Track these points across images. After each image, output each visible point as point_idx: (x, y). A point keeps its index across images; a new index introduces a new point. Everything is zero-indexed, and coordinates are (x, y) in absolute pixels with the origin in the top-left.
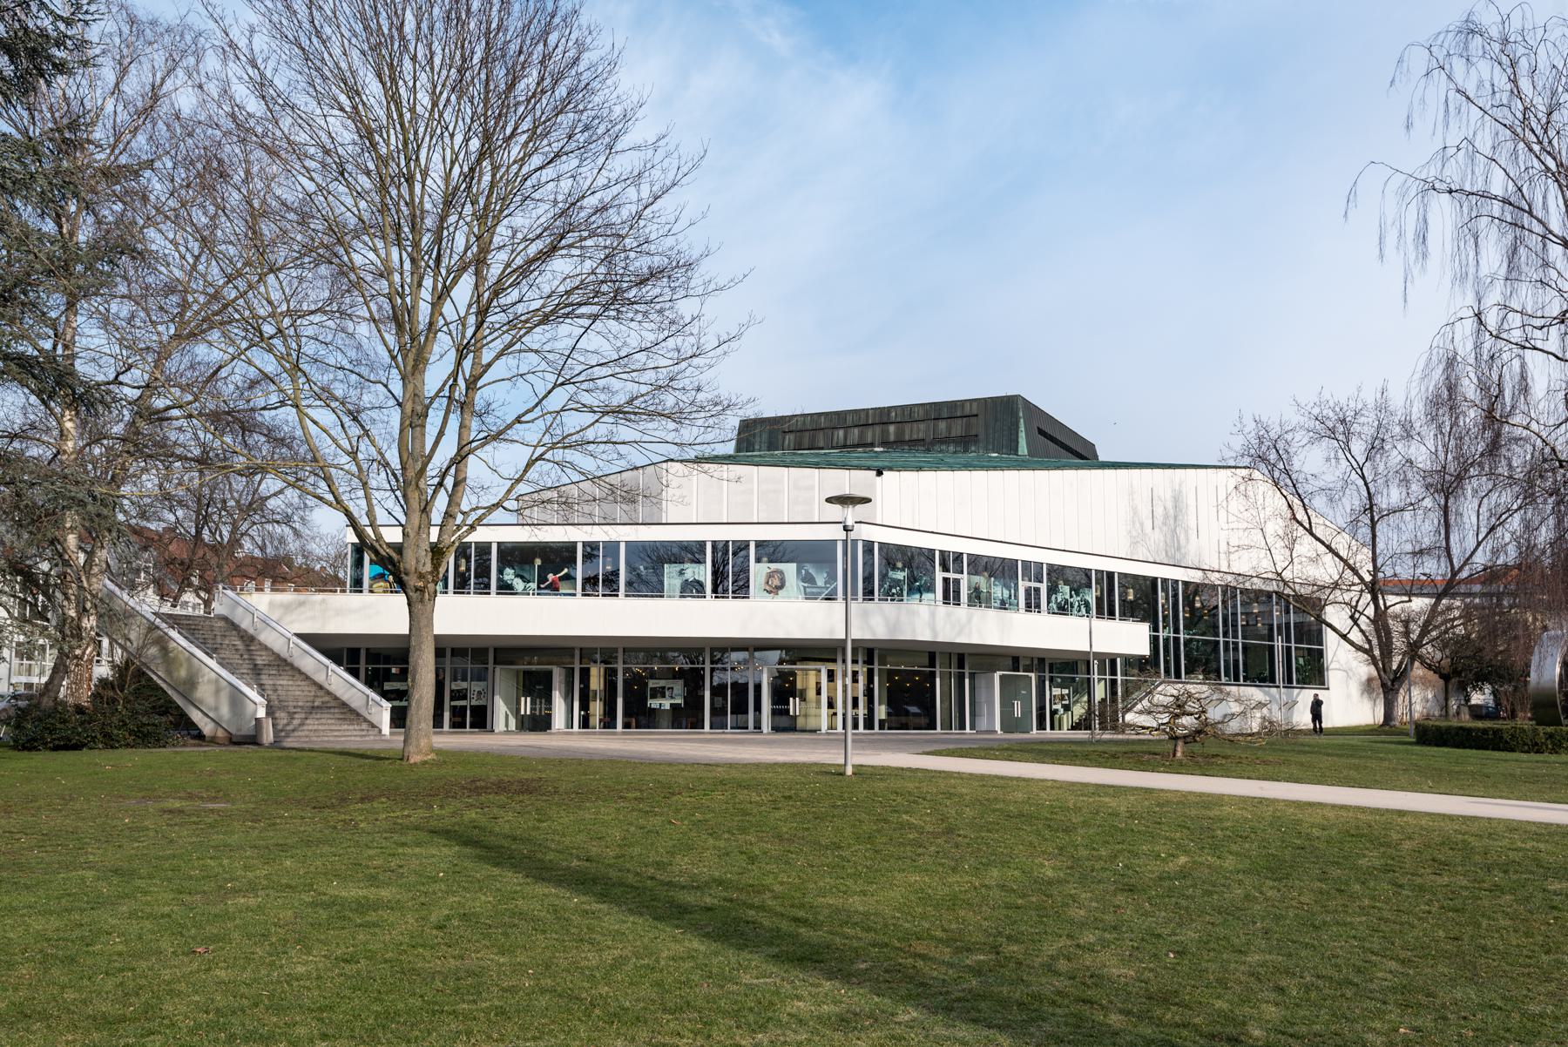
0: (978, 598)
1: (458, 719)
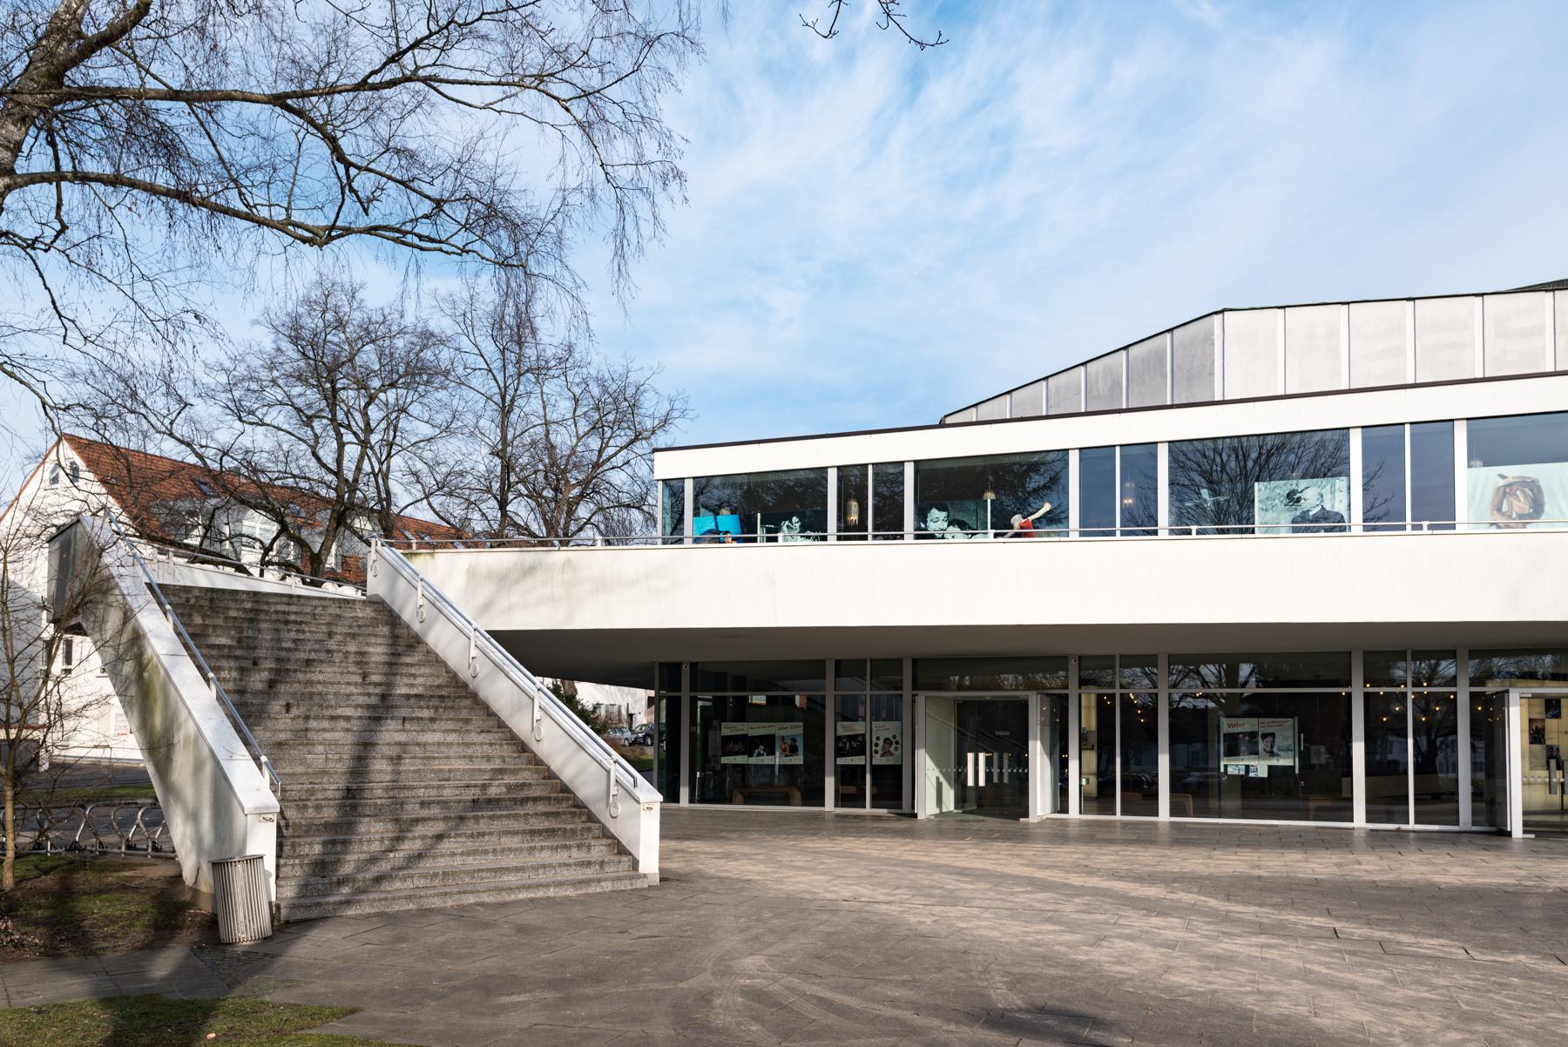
1: (852, 790)
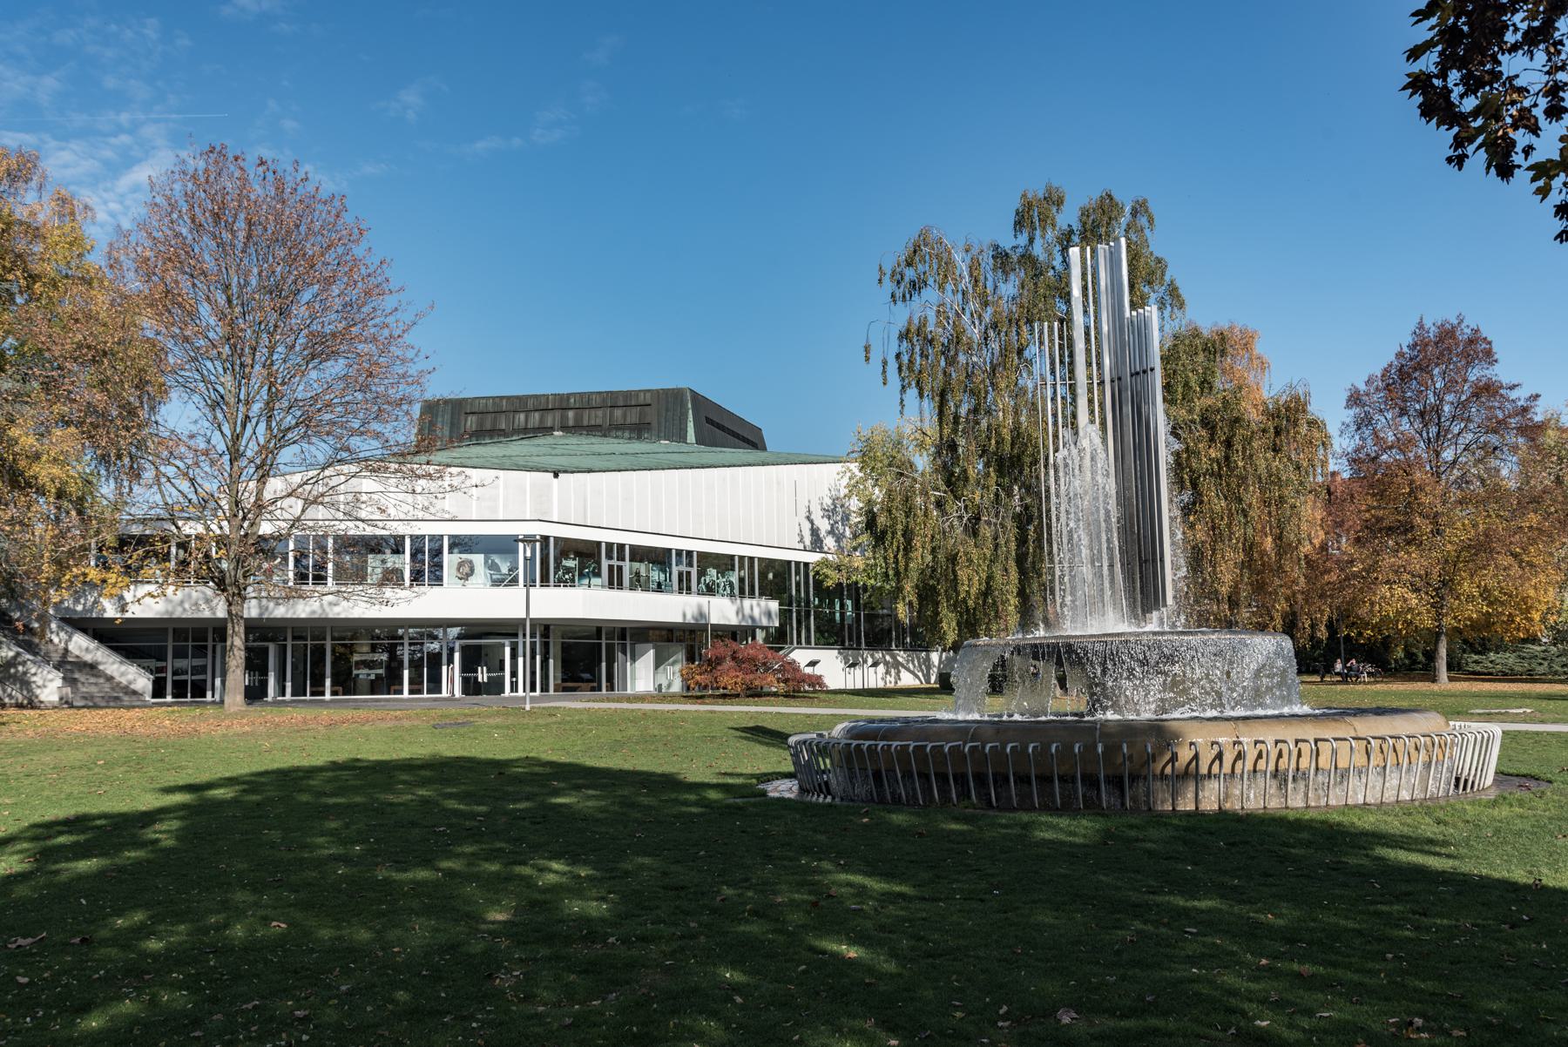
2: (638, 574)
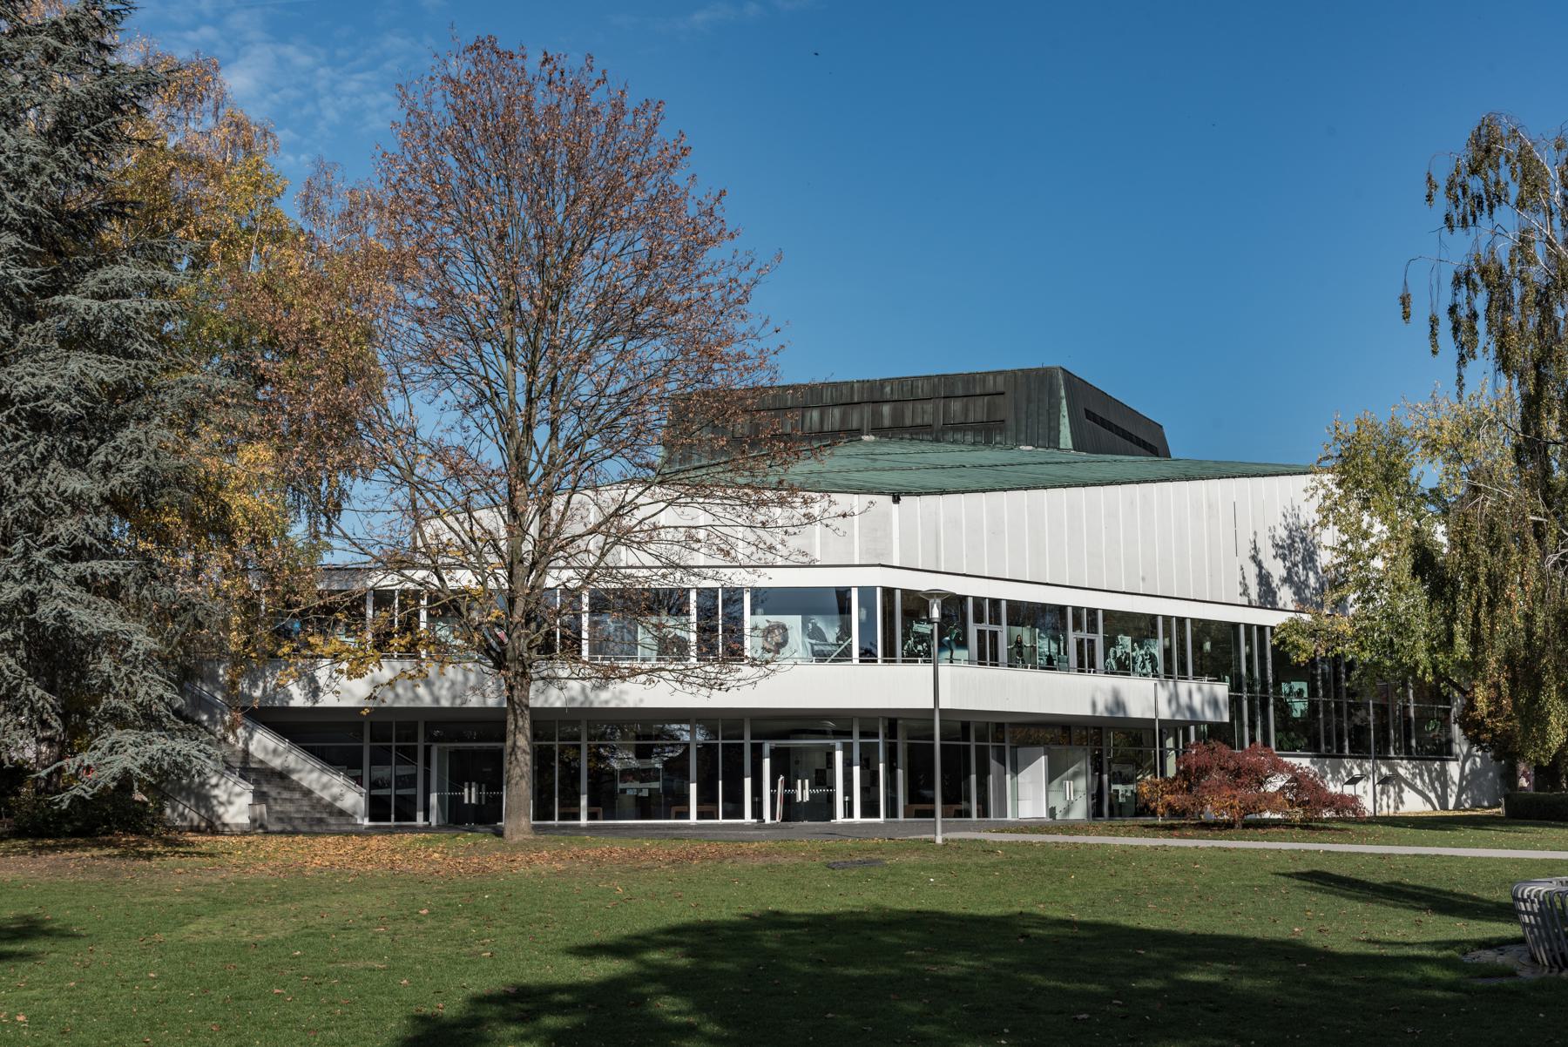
0: (1020, 654)
2: (1019, 644)
